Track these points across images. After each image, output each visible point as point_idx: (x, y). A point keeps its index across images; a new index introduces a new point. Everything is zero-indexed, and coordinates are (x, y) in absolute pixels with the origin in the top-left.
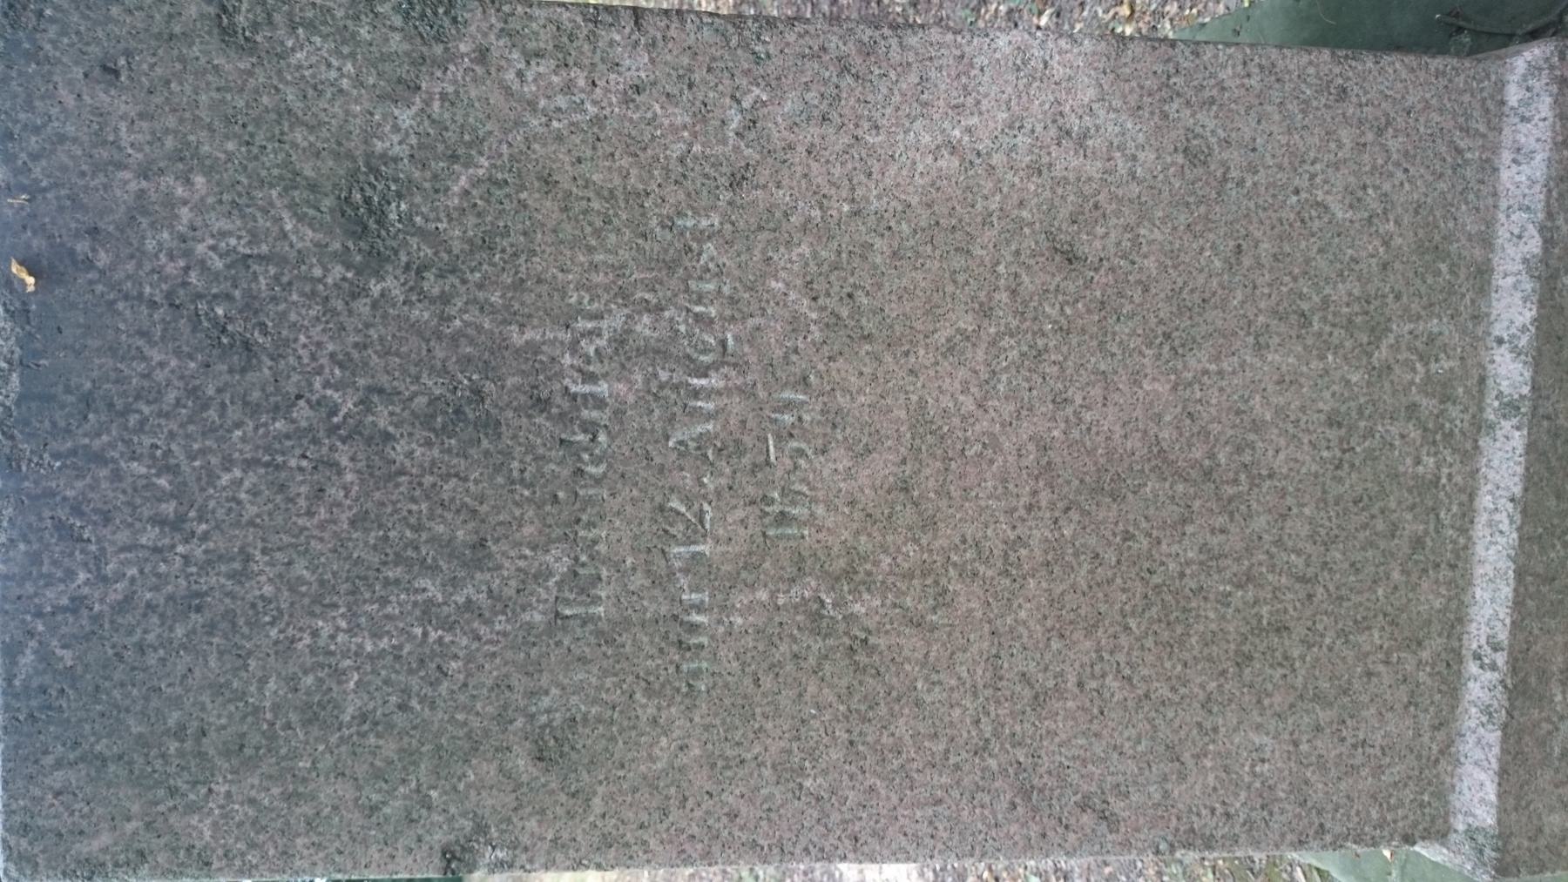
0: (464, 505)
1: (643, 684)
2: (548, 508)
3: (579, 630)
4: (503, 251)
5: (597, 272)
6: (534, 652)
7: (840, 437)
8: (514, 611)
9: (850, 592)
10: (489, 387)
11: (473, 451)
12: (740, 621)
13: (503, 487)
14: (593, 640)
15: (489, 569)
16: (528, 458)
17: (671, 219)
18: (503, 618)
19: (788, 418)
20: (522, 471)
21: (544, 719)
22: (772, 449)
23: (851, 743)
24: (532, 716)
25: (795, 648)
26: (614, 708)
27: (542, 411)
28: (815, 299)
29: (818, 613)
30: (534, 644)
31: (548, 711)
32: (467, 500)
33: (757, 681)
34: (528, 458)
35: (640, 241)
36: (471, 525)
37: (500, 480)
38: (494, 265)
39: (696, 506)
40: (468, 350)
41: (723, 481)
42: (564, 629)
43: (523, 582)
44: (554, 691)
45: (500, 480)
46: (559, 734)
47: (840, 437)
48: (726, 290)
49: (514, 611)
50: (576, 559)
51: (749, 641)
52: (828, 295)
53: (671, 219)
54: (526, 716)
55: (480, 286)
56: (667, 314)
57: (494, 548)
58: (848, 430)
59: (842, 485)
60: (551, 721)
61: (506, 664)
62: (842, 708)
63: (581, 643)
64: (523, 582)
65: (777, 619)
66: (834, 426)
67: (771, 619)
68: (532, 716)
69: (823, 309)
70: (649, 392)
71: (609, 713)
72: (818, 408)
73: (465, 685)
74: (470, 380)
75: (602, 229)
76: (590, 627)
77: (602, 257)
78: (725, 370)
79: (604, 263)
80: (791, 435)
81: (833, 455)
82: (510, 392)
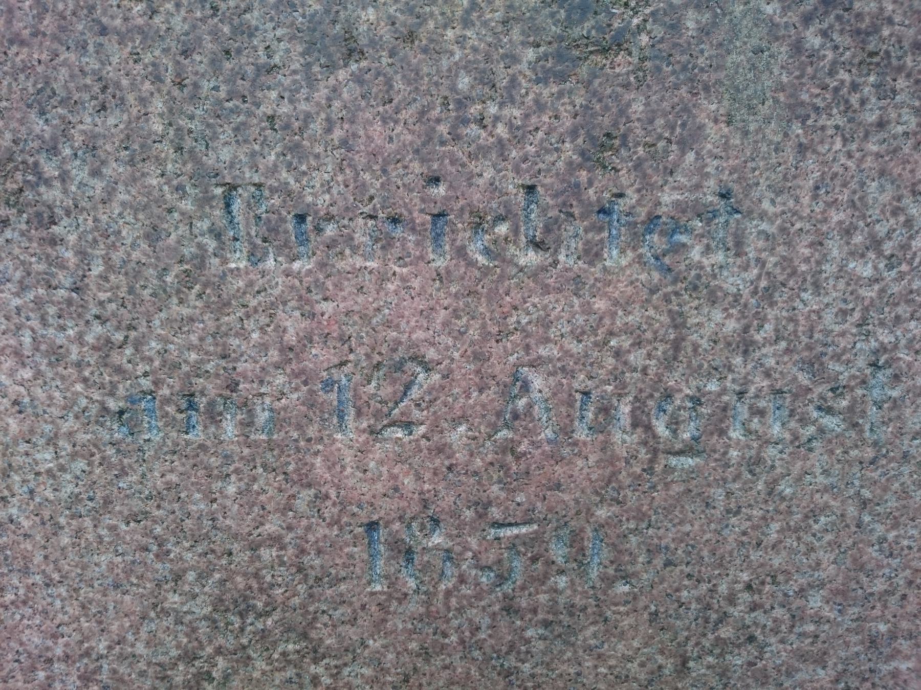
0: (422, 19)
1: (119, 337)
2: (416, 167)
3: (205, 225)
4: (855, 87)
5: (811, 245)
6: (166, 149)
7: (529, 633)
8: (235, 111)
9: (284, 654)
10: (623, 64)
11: (516, 34)
12: (231, 490)
13: (453, 88)
14: (189, 250)
15: (308, 66)
16: (501, 130)
17: (888, 364)
18: (222, 94)
19: (558, 552)
20: (480, 121)
21: (50, 169)
22: (516, 531)
23: (50, 661)
24: (53, 150)
25: (191, 576)
26: (76, 290)
27: (582, 154)
28: (749, 587)
29: (250, 608)
30: (179, 149)
31: (64, 177)
32: (431, 25)
33: (133, 518)
34: (501, 130)
35: (857, 315)
36: (385, 31)
37: (464, 82)
38: (832, 73)
39: (416, 414)
40: (691, 24)
41: (461, 457)
42: (206, 200)
43: (287, 127)
44: (99, 185)
45: (464, 82)
46: (29, 195)
47: (529, 633)
48: (771, 452)
49: (235, 111)
50: (329, 218)
51: (199, 505)
52: (754, 607)
53: (888, 364)
54: (54, 139)
55: (797, 47)
56: (738, 360)
57: (342, 74)
58: (541, 645)
59: (454, 638)
60: (48, 183)
61: (143, 101)
62: (102, 647)
63: (183, 229)
64: (287, 127)
65: (236, 547)
66: (546, 624)
67: (236, 536)
68: (53, 150)
69: (731, 599)
70: (611, 333)
71: (68, 283)
72: (578, 600)
73: (103, 31)
74: (640, 29)
75: (880, 254)
76: (211, 244)
77: (835, 252)
78: (643, 454)
79: (824, 258)
80: (534, 560)
81: (503, 623)
82: (617, 97)
